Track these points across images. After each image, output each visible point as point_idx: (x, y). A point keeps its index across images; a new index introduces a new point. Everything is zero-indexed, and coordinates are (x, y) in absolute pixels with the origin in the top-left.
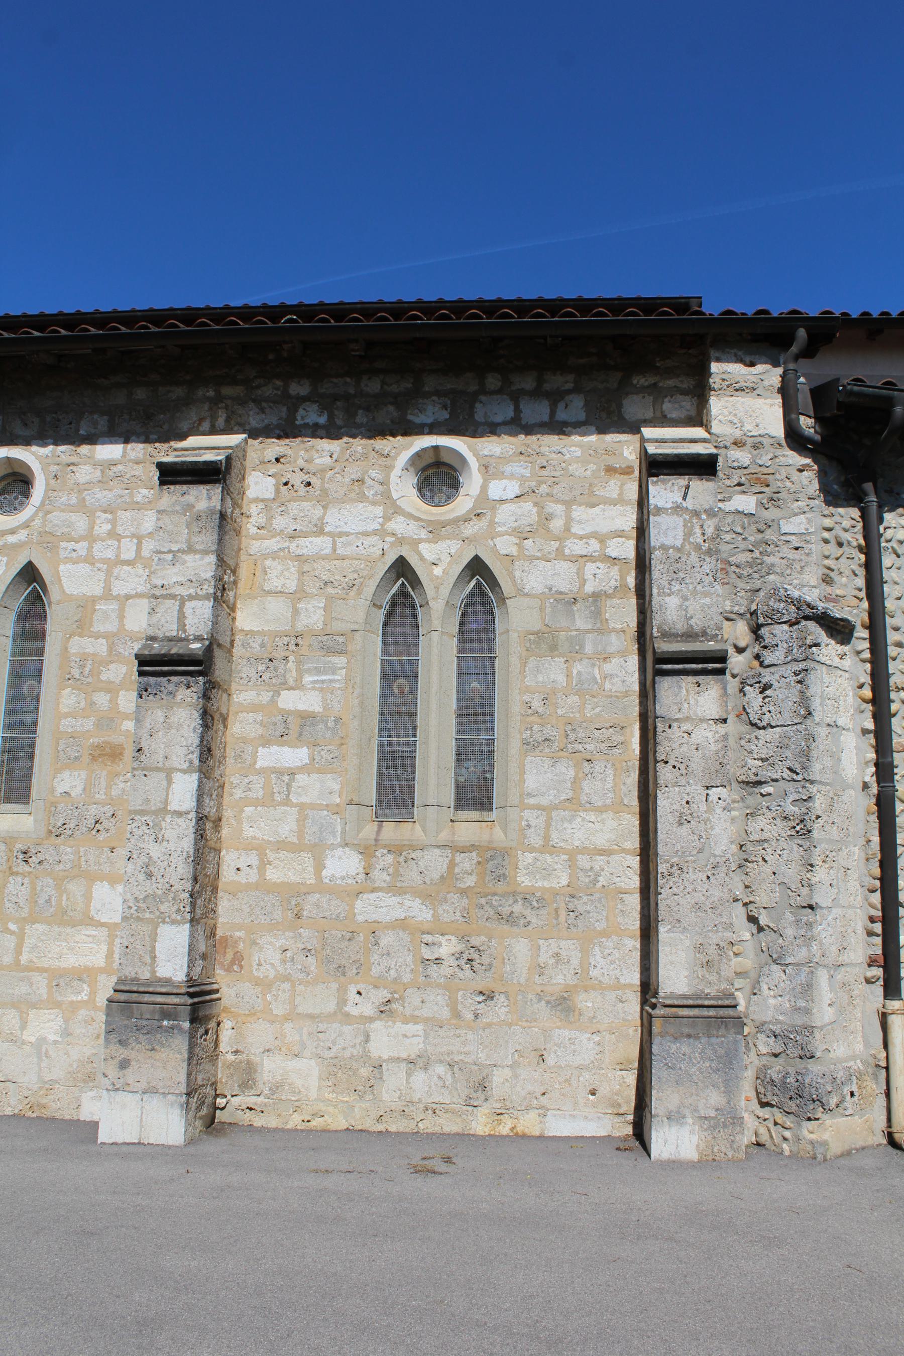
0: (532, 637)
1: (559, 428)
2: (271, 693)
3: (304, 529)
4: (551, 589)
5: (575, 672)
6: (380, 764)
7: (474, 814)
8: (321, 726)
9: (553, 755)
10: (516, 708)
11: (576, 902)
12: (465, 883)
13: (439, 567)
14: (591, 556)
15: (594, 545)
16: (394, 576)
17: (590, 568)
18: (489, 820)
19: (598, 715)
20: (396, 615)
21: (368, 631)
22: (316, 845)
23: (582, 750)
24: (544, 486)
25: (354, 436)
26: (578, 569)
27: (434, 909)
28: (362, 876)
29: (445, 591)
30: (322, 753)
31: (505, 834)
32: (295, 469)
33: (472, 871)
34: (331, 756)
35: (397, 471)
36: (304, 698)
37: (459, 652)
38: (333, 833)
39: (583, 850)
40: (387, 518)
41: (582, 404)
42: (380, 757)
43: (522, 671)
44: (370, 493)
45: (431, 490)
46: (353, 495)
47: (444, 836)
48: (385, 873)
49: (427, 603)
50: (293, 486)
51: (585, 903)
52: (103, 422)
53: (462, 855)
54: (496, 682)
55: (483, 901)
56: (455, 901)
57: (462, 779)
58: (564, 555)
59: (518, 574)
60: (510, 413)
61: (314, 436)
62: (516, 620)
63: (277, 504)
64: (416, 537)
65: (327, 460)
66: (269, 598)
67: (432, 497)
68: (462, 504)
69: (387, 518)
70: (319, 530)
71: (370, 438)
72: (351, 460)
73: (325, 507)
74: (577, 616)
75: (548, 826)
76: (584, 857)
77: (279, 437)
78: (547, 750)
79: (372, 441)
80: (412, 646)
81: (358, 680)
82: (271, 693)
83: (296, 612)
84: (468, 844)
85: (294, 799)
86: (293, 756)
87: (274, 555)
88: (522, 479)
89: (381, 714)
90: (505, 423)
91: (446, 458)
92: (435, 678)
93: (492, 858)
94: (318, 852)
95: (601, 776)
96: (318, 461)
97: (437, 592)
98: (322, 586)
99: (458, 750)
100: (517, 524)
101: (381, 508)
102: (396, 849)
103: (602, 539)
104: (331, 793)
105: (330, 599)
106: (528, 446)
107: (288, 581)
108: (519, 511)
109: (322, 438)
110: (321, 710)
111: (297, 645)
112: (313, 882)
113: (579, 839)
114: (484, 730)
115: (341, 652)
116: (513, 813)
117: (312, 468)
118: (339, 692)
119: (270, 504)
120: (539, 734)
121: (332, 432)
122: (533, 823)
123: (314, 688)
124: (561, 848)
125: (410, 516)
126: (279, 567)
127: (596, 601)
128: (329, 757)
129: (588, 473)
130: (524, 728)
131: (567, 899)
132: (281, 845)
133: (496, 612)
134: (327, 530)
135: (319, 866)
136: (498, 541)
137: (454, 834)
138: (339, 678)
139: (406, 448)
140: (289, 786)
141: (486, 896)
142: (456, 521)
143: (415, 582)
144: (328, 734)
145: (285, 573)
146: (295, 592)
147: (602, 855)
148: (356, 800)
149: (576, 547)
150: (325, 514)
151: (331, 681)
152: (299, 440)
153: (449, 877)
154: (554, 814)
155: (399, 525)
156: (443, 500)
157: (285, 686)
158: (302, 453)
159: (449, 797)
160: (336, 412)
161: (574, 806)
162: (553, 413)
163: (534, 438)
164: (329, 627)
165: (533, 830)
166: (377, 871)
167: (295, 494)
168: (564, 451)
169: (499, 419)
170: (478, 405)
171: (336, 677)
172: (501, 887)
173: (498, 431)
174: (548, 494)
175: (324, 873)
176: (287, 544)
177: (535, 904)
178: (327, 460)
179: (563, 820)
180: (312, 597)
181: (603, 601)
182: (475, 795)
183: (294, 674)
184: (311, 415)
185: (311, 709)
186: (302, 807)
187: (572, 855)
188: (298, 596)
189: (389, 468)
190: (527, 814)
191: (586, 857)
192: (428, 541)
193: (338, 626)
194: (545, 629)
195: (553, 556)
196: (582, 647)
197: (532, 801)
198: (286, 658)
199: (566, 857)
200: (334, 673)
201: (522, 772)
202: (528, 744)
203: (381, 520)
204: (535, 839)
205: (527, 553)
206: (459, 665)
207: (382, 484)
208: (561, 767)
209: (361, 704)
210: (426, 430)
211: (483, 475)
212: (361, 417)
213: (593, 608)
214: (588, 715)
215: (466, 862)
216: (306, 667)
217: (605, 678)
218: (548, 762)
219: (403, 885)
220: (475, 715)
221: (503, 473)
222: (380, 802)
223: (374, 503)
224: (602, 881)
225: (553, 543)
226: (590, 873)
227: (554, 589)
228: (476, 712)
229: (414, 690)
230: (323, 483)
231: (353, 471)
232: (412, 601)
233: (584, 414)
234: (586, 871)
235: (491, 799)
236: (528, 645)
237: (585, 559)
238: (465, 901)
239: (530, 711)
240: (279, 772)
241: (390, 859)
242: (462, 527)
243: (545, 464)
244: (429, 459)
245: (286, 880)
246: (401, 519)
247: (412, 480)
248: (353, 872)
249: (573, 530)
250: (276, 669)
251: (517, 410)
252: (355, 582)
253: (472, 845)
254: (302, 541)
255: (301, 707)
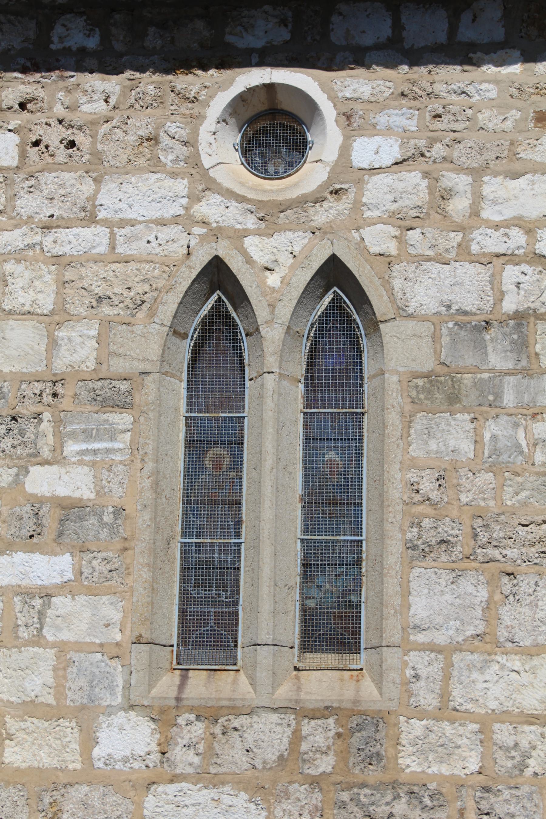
0: (420, 382)
1: (465, 54)
2: (15, 470)
3: (65, 215)
4: (449, 307)
5: (487, 436)
6: (184, 580)
7: (330, 659)
8: (93, 520)
9: (454, 565)
10: (396, 492)
11: (493, 799)
12: (317, 767)
13: (276, 271)
14: (513, 255)
15: (518, 238)
16: (205, 287)
17: (511, 273)
18: (354, 666)
19: (524, 504)
20: (209, 348)
21: (166, 373)
22: (83, 707)
23: (500, 557)
24: (439, 145)
25: (142, 70)
26: (493, 275)
27: (268, 810)
28: (156, 757)
29: (285, 311)
30: (95, 563)
31: (380, 689)
32: (51, 121)
33: (329, 748)
34: (108, 567)
35: (209, 124)
36: (65, 477)
37: (307, 406)
38: (111, 688)
39: (503, 716)
40: (194, 198)
41: (499, 14)
42: (184, 569)
43: (406, 434)
44: (167, 159)
45: (262, 154)
46: (141, 162)
47: (284, 692)
48: (192, 752)
49: (257, 330)
50: (47, 147)
51: (507, 801)
52: (517, 53)
53: (313, 722)
54: (365, 451)
55: (345, 796)
56: (302, 796)
57: (311, 603)
58: (469, 253)
59: (397, 284)
60: (385, 30)
61: (80, 68)
62: (398, 355)
63: (23, 176)
64: (239, 227)
65: (100, 107)
66: (11, 322)
67: (264, 165)
68: (311, 175)
69: (194, 198)
70: (89, 217)
71: (167, 71)
72: (137, 106)
73: (97, 181)
74: (490, 349)
75: (447, 677)
76: (504, 727)
77: (24, 70)
78: (444, 558)
79: (170, 77)
80: (234, 398)
81: (150, 449)
82: (15, 470)
83: (53, 343)
84: (322, 705)
85: (49, 634)
86: (49, 568)
87: (19, 256)
88: (405, 135)
89: (187, 502)
90: (378, 47)
91: (286, 104)
92: (269, 446)
93: (360, 727)
94: (86, 718)
95: (529, 599)
96: (86, 108)
97: (272, 312)
98: (95, 304)
99: (305, 558)
100: (396, 206)
101: (186, 181)
102: (209, 714)
103: (530, 229)
104: (107, 626)
105: (107, 323)
106: (413, 83)
107: (40, 296)
108: (400, 186)
109: (91, 72)
110: (92, 496)
111: (55, 395)
112: (78, 766)
113: (496, 699)
114: (345, 526)
115: (124, 406)
116: (391, 657)
117: (76, 118)
118: (121, 468)
119: (11, 175)
120: (432, 533)
121: (107, 63)
122: (423, 672)
123: (81, 463)
124: (466, 711)
125: (230, 194)
126: (27, 275)
127: (519, 325)
128: (105, 568)
129: (509, 124)
130: (407, 524)
131: (478, 794)
132: (30, 708)
133: (365, 343)
134: (101, 215)
135: (89, 741)
136: (366, 232)
137: (299, 689)
138: (121, 446)
139: (223, 87)
140: (41, 614)
141: (349, 788)
142: (301, 202)
143: (238, 296)
144: (104, 534)
145: (37, 283)
146: (52, 313)
147: (533, 724)
148: (147, 636)
149: (488, 242)
150: (97, 191)
151: (108, 451)
152: (55, 74)
153: (292, 757)
154: (456, 658)
155: (212, 208)
156: (282, 169)
157: (36, 458)
158: (61, 95)
159: (292, 630)
160: (114, 31)
161: (488, 646)
162: (453, 30)
163: (423, 70)
164: (104, 366)
165: (422, 683)
166: (178, 748)
167: (50, 160)
168: (470, 89)
169: (368, 40)
170: (335, 19)
171: (117, 445)
172: (373, 774)
173: (367, 60)
174: (444, 158)
175: (96, 752)
176: (38, 238)
177: (427, 801)
178: (100, 107)
179: (470, 668)
180: (78, 321)
181: (531, 325)
182: (333, 628)
183: (51, 439)
184: (75, 34)
185: (77, 495)
186: (62, 648)
187: (485, 724)
188: (55, 319)
189: (197, 119)
190: (413, 657)
191: (507, 727)
192: (258, 233)
193: (119, 366)
194: (440, 369)
195: (453, 255)
196: (498, 396)
197: (421, 638)
198: (38, 416)
199: (475, 727)
200: (112, 438)
201: (406, 592)
202: (414, 548)
203: (185, 201)
204: (427, 699)
205: (411, 250)
206: (306, 425)
207: (186, 144)
208: (467, 585)
209: (156, 486)
210: (255, 58)
211: (343, 129)
212: (153, 39)
213: (515, 337)
214: (509, 503)
215: (319, 735)
216: (68, 429)
217: (535, 445)
218: (446, 576)
219: (221, 770)
220: (332, 502)
221: (374, 126)
222: (184, 638)
223: (174, 175)
224: (534, 765)
225: (452, 234)
226: (513, 753)
227: (455, 307)
228: (333, 500)
229: (237, 464)
230: (94, 143)
231: (141, 124)
232: (233, 326)
233: (502, 31)
234: (508, 749)
235: (357, 634)
236: (414, 394)
237: (502, 260)
238: (317, 797)
239: (417, 498)
240: (27, 594)
241: (199, 728)
242: (311, 211)
243: (440, 110)
244: (259, 105)
245: (36, 764)
246: (215, 199)
247: (232, 137)
248: (141, 750)
249: (484, 215)
250: (22, 433)
251: (397, 26)
252: (145, 298)
253: (327, 708)
254: (62, 234)
255: (62, 491)
